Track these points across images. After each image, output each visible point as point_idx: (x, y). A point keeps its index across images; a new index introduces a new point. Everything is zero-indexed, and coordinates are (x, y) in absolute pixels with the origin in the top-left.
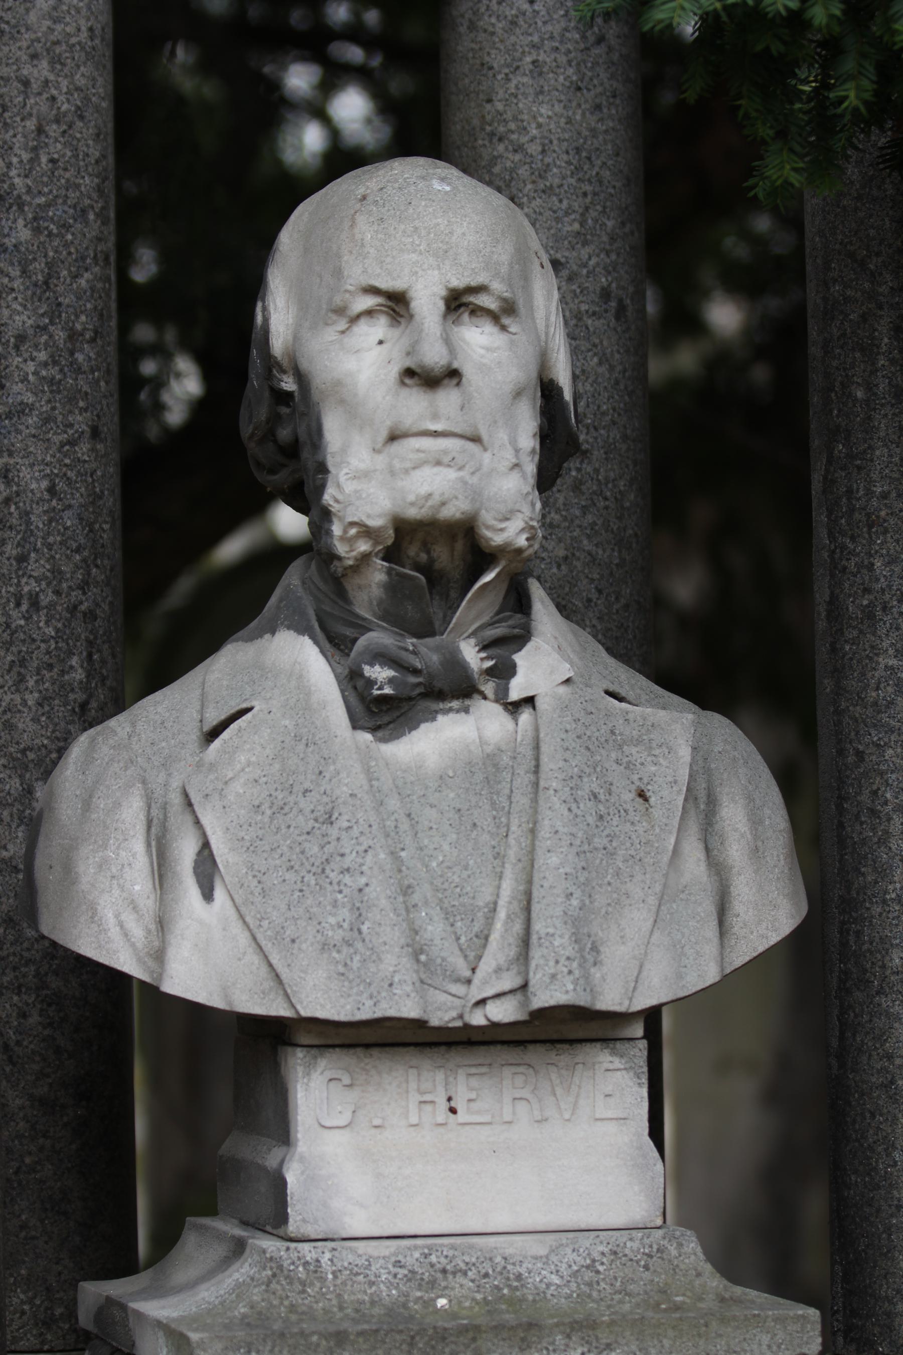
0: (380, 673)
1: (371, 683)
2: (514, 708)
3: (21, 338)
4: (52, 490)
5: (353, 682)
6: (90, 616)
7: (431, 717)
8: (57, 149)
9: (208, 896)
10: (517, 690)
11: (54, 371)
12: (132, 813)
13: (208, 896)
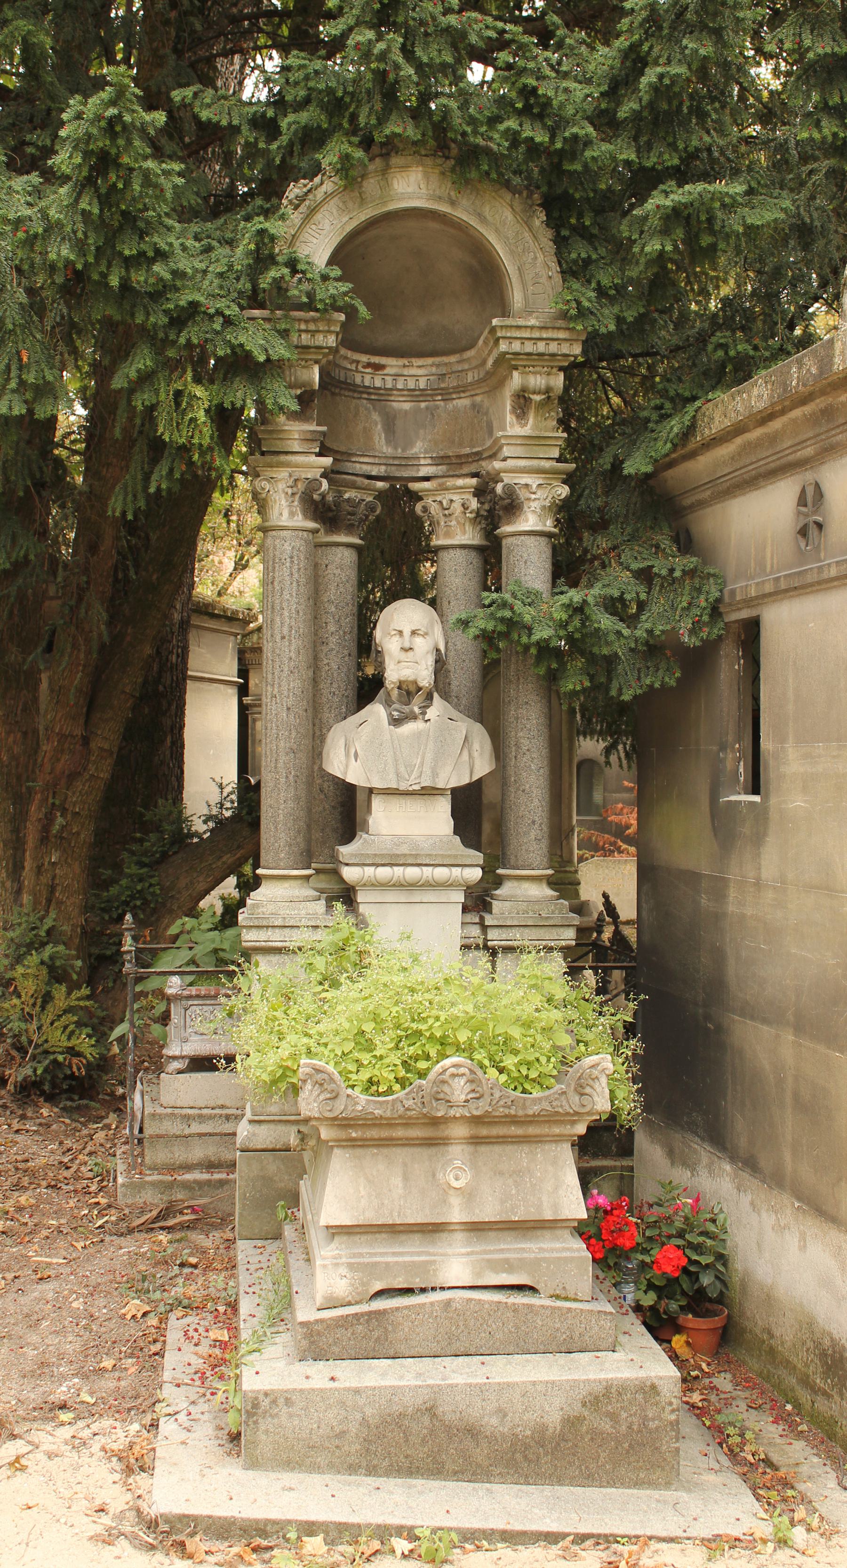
5: (390, 715)
12: (342, 742)
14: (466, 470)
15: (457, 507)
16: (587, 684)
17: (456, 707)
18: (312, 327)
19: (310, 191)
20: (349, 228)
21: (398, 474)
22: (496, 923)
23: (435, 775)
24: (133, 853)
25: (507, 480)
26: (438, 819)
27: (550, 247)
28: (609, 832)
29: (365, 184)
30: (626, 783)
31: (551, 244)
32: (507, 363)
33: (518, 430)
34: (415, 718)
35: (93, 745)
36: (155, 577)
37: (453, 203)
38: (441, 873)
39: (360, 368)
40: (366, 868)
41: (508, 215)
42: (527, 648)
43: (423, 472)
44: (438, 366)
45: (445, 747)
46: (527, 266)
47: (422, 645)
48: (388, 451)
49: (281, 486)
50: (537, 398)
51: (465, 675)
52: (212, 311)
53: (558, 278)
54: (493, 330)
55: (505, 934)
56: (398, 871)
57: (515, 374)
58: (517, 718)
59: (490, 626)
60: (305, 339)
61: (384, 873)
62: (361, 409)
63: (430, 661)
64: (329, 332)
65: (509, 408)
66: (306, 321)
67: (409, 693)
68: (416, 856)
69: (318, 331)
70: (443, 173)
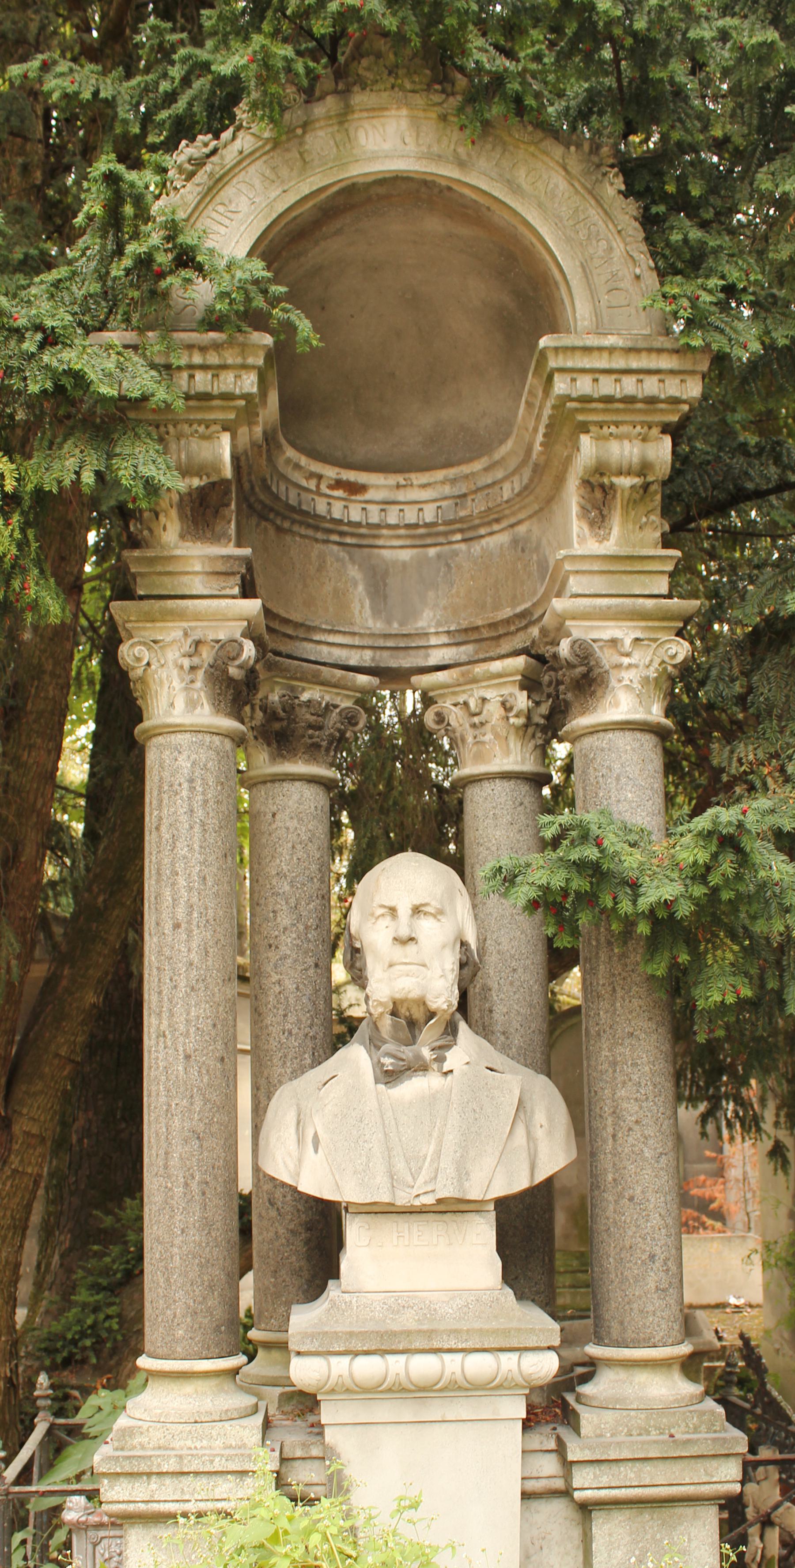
0: (387, 1061)
1: (383, 1065)
2: (446, 1074)
3: (285, 929)
4: (297, 988)
6: (314, 1038)
7: (410, 1077)
8: (300, 854)
9: (316, 1151)
10: (446, 1067)
11: (299, 942)
12: (291, 1118)
13: (316, 1151)
14: (506, 646)
15: (494, 711)
16: (747, 992)
17: (504, 1049)
18: (213, 359)
19: (214, 152)
20: (281, 208)
21: (393, 664)
22: (587, 1455)
23: (462, 1174)
24: (90, 1272)
25: (576, 634)
26: (472, 1258)
27: (635, 231)
28: (691, 1206)
29: (308, 138)
30: (708, 1153)
31: (637, 225)
32: (569, 421)
33: (593, 547)
34: (424, 1068)
35: (16, 1129)
36: (101, 899)
37: (462, 164)
38: (480, 1365)
39: (324, 489)
40: (334, 1360)
41: (559, 181)
42: (629, 923)
43: (436, 657)
44: (453, 481)
45: (487, 1121)
46: (597, 262)
47: (434, 934)
48: (378, 626)
49: (172, 655)
50: (625, 482)
51: (513, 988)
52: (22, 322)
53: (651, 280)
54: (543, 354)
55: (605, 1476)
56: (396, 1364)
57: (585, 440)
58: (614, 1064)
59: (557, 881)
60: (202, 381)
61: (368, 1368)
62: (329, 560)
63: (450, 962)
64: (244, 367)
65: (575, 509)
66: (203, 349)
67: (412, 1024)
68: (430, 1334)
69: (224, 367)
70: (443, 118)
